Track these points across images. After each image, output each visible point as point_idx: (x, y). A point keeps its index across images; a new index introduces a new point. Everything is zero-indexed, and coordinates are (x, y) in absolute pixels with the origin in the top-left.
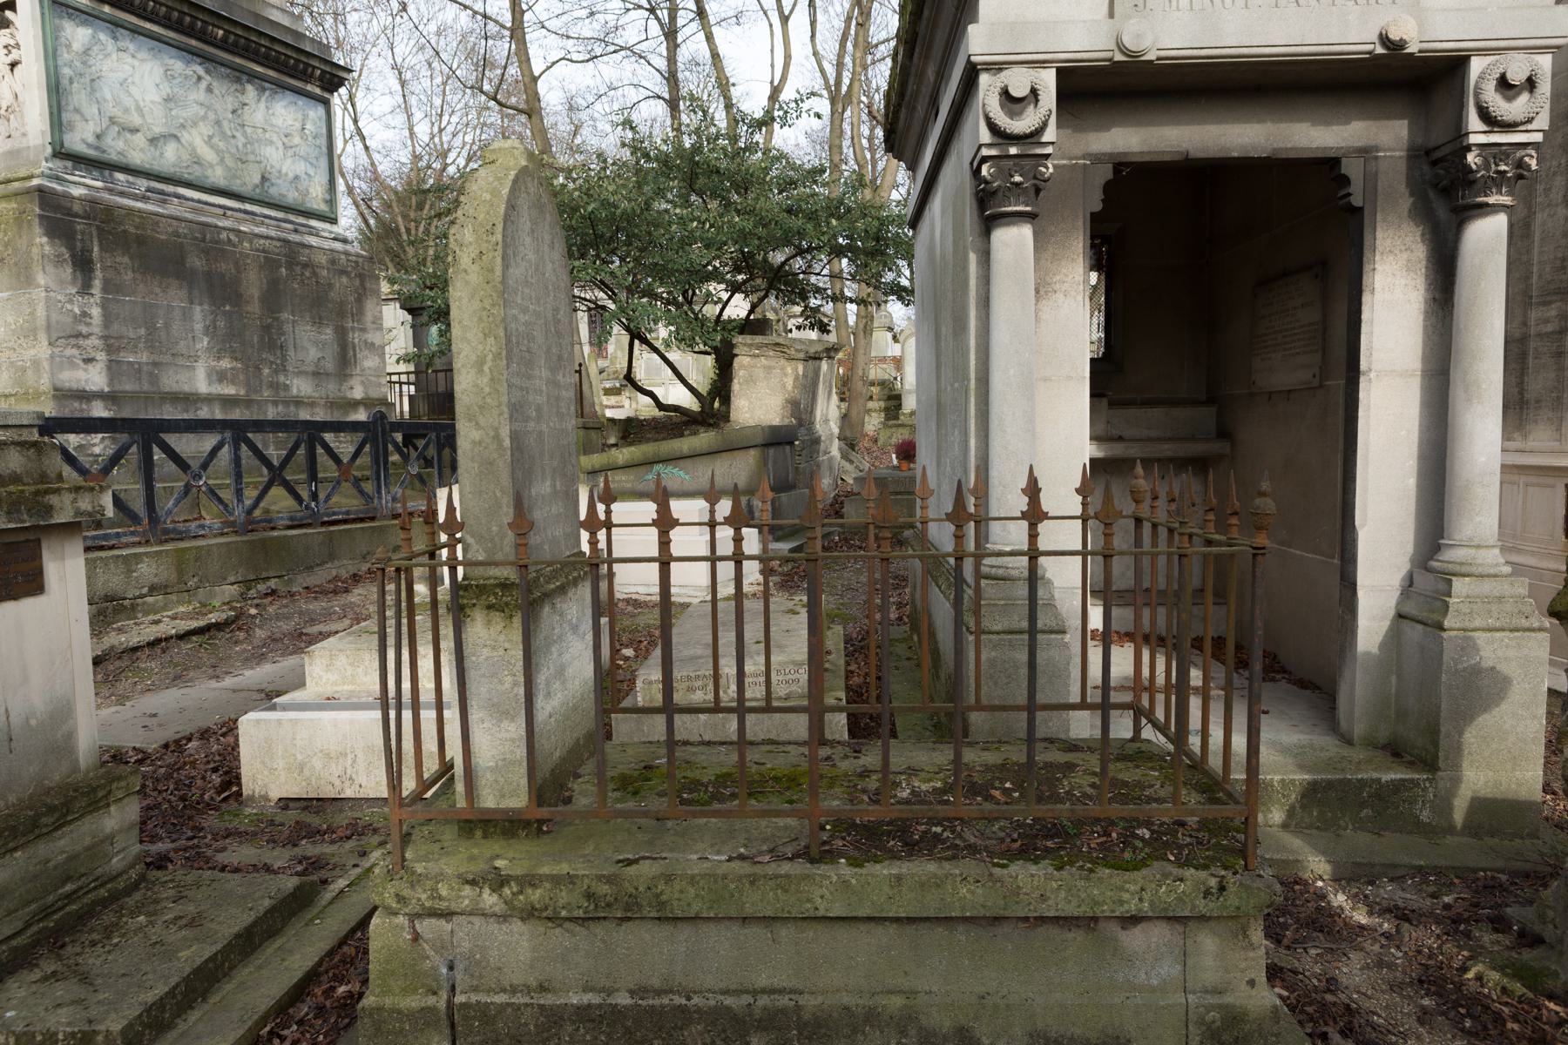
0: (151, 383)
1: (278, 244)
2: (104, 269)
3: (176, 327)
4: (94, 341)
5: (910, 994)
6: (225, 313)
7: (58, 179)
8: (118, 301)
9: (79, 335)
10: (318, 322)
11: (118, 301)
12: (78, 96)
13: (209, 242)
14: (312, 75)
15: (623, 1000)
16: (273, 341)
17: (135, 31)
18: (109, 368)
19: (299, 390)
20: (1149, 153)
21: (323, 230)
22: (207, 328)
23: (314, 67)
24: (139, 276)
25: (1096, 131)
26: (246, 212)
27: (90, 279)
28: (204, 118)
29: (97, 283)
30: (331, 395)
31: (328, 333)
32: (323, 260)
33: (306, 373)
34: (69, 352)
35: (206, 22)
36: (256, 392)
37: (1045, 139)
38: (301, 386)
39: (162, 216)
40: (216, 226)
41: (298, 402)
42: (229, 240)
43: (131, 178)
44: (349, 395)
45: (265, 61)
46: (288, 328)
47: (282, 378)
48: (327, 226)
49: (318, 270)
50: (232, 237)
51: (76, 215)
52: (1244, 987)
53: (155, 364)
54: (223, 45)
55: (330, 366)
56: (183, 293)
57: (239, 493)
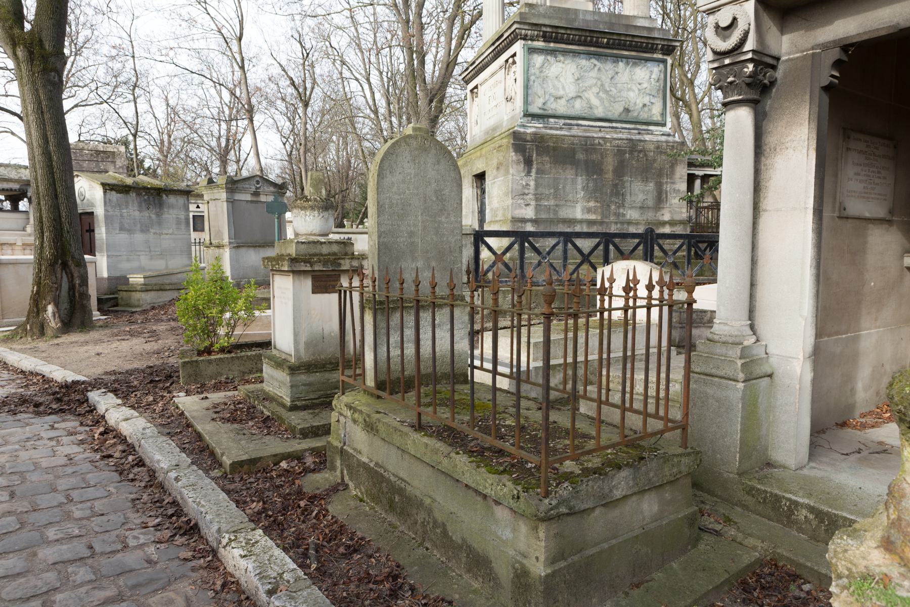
0: (554, 214)
1: (626, 142)
2: (537, 164)
3: (568, 188)
4: (531, 196)
5: (434, 500)
6: (593, 180)
7: (524, 126)
8: (542, 178)
9: (524, 194)
10: (646, 180)
11: (542, 178)
12: (536, 88)
13: (589, 145)
14: (656, 49)
15: (372, 465)
16: (619, 191)
17: (565, 52)
18: (536, 208)
19: (630, 216)
20: (865, 33)
21: (656, 131)
22: (583, 188)
23: (657, 44)
24: (553, 165)
25: (823, 27)
26: (613, 128)
27: (531, 169)
28: (596, 85)
29: (534, 170)
30: (650, 219)
31: (651, 186)
32: (652, 147)
33: (635, 207)
34: (520, 201)
35: (598, 38)
36: (606, 217)
37: (745, 49)
38: (632, 214)
39: (567, 136)
40: (593, 137)
41: (629, 223)
42: (599, 143)
43: (556, 120)
44: (661, 218)
45: (630, 48)
46: (627, 184)
47: (621, 211)
48: (660, 128)
49: (647, 153)
50: (601, 141)
51: (528, 141)
52: (534, 559)
53: (557, 206)
54: (607, 46)
55: (650, 203)
56: (573, 172)
57: (565, 266)
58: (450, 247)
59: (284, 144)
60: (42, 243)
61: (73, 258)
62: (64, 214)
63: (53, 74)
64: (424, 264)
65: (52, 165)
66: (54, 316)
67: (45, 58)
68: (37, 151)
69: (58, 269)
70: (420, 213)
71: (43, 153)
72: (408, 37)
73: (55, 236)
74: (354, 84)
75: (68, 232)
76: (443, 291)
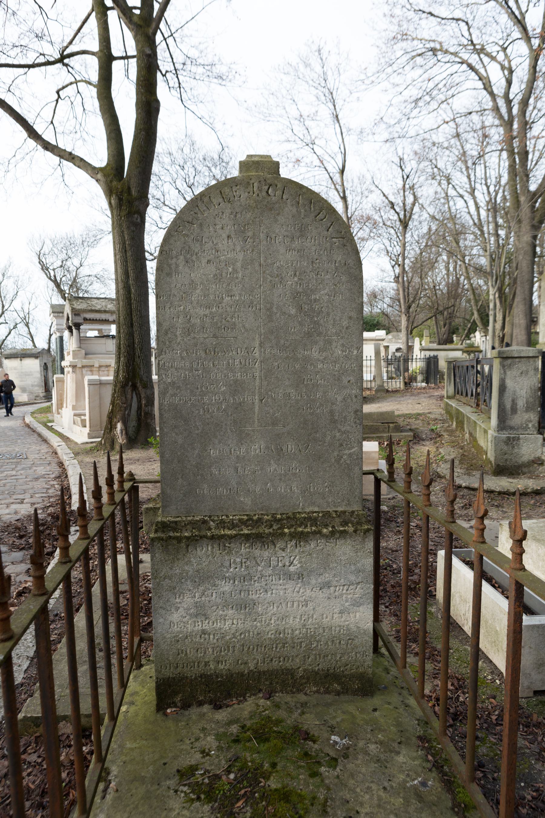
58: (332, 412)
59: (393, 267)
60: (119, 367)
61: (141, 380)
62: (137, 340)
63: (136, 216)
64: (267, 448)
65: (130, 297)
66: (122, 433)
67: (130, 203)
68: (121, 285)
69: (129, 390)
70: (257, 343)
71: (124, 287)
72: (509, 139)
73: (128, 360)
74: (460, 203)
75: (139, 357)
76: (313, 504)
